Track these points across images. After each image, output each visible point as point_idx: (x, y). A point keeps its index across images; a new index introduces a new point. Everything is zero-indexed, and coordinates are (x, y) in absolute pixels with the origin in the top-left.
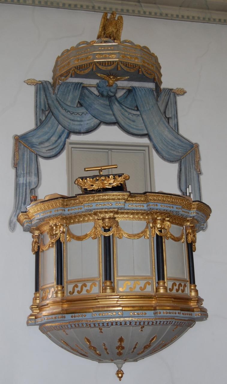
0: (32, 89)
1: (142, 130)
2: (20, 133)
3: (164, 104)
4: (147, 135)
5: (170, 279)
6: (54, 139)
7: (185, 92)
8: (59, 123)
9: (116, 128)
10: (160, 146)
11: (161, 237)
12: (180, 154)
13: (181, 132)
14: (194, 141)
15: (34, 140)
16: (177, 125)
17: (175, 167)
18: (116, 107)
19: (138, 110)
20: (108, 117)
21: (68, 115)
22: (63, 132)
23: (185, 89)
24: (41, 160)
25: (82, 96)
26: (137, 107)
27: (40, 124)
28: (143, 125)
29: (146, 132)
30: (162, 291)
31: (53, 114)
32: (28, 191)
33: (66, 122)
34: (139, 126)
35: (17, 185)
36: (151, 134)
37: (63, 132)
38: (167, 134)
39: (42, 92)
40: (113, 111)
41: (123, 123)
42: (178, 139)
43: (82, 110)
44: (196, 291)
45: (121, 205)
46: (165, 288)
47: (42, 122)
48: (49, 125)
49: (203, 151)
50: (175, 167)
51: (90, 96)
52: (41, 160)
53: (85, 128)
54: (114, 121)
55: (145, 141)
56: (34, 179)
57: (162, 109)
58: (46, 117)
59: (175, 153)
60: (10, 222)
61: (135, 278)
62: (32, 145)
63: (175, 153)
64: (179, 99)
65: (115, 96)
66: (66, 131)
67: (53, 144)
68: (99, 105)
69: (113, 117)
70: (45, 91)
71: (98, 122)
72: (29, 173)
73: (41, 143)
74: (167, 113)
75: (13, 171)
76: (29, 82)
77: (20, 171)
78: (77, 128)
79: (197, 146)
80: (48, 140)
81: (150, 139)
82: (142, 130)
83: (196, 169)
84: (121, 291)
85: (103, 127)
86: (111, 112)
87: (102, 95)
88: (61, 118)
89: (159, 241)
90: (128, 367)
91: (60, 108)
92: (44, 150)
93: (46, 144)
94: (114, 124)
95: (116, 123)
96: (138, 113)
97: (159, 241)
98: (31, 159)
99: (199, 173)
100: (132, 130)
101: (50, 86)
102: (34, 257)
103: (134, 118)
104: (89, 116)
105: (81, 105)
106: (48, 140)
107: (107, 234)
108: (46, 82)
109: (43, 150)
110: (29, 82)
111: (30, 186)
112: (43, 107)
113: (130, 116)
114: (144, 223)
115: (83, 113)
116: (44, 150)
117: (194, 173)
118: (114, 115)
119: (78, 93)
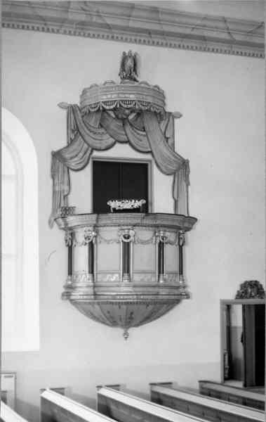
0: (64, 112)
1: (147, 148)
2: (56, 149)
3: (164, 127)
4: (150, 152)
5: (169, 273)
6: (81, 154)
7: (181, 116)
8: (85, 141)
9: (127, 146)
10: (159, 161)
11: (163, 244)
12: (174, 169)
13: (176, 150)
14: (186, 158)
15: (67, 156)
16: (173, 144)
17: (171, 178)
18: (128, 129)
19: (144, 131)
20: (123, 136)
21: (91, 134)
22: (87, 149)
23: (182, 113)
24: (70, 171)
25: (102, 119)
26: (144, 128)
27: (71, 142)
28: (148, 144)
29: (149, 150)
30: (161, 281)
31: (80, 134)
32: (62, 197)
33: (91, 141)
34: (144, 144)
35: (54, 192)
36: (154, 152)
37: (87, 149)
38: (166, 152)
39: (72, 115)
40: (125, 131)
41: (132, 141)
42: (174, 155)
43: (102, 130)
44: (183, 280)
45: (139, 221)
46: (165, 280)
47: (72, 141)
48: (78, 143)
49: (192, 166)
50: (171, 178)
51: (109, 118)
52: (72, 173)
53: (103, 147)
54: (127, 140)
55: (149, 157)
56: (66, 188)
57: (163, 130)
58: (75, 136)
59: (171, 167)
60: (50, 222)
61: (144, 272)
62: (64, 160)
63: (171, 167)
64: (177, 121)
65: (127, 118)
66: (90, 149)
67: (81, 159)
68: (114, 125)
69: (125, 137)
70: (74, 113)
71: (114, 141)
72: (63, 183)
73: (72, 158)
74: (167, 133)
75: (51, 181)
76: (61, 106)
77: (56, 181)
78: (98, 146)
79: (188, 162)
80: (77, 155)
81: (153, 156)
82: (147, 148)
83: (185, 181)
84: (110, 202)
85: (118, 145)
86: (124, 133)
87: (117, 116)
88: (87, 138)
89: (161, 246)
90: (133, 331)
91: (85, 129)
92: (73, 164)
93: (76, 159)
94: (126, 142)
95: (128, 142)
96: (144, 133)
97: (161, 246)
98: (64, 172)
99: (188, 184)
100: (141, 149)
101: (77, 109)
102: (66, 250)
103: (142, 137)
104: (108, 136)
105: (101, 126)
106: (77, 155)
107: (126, 241)
108: (74, 105)
109: (73, 164)
110: (61, 106)
111: (64, 192)
112: (73, 127)
113: (138, 136)
114: (152, 233)
115: (103, 133)
116: (73, 164)
117: (184, 184)
118: (126, 135)
119: (99, 116)
